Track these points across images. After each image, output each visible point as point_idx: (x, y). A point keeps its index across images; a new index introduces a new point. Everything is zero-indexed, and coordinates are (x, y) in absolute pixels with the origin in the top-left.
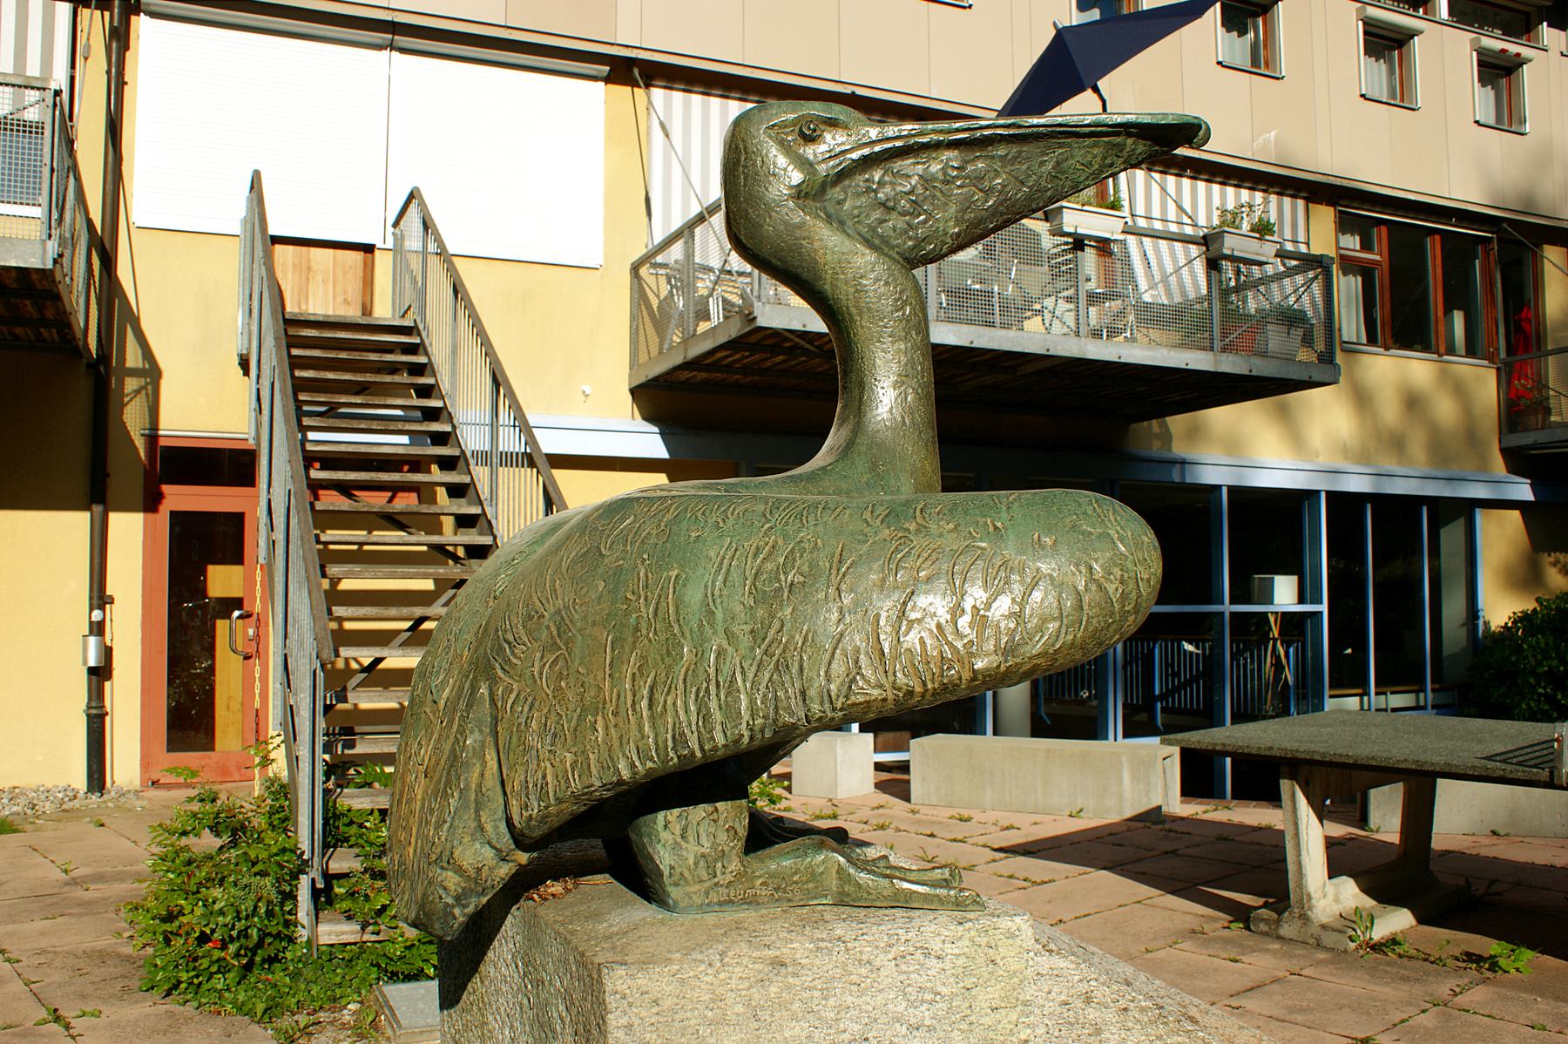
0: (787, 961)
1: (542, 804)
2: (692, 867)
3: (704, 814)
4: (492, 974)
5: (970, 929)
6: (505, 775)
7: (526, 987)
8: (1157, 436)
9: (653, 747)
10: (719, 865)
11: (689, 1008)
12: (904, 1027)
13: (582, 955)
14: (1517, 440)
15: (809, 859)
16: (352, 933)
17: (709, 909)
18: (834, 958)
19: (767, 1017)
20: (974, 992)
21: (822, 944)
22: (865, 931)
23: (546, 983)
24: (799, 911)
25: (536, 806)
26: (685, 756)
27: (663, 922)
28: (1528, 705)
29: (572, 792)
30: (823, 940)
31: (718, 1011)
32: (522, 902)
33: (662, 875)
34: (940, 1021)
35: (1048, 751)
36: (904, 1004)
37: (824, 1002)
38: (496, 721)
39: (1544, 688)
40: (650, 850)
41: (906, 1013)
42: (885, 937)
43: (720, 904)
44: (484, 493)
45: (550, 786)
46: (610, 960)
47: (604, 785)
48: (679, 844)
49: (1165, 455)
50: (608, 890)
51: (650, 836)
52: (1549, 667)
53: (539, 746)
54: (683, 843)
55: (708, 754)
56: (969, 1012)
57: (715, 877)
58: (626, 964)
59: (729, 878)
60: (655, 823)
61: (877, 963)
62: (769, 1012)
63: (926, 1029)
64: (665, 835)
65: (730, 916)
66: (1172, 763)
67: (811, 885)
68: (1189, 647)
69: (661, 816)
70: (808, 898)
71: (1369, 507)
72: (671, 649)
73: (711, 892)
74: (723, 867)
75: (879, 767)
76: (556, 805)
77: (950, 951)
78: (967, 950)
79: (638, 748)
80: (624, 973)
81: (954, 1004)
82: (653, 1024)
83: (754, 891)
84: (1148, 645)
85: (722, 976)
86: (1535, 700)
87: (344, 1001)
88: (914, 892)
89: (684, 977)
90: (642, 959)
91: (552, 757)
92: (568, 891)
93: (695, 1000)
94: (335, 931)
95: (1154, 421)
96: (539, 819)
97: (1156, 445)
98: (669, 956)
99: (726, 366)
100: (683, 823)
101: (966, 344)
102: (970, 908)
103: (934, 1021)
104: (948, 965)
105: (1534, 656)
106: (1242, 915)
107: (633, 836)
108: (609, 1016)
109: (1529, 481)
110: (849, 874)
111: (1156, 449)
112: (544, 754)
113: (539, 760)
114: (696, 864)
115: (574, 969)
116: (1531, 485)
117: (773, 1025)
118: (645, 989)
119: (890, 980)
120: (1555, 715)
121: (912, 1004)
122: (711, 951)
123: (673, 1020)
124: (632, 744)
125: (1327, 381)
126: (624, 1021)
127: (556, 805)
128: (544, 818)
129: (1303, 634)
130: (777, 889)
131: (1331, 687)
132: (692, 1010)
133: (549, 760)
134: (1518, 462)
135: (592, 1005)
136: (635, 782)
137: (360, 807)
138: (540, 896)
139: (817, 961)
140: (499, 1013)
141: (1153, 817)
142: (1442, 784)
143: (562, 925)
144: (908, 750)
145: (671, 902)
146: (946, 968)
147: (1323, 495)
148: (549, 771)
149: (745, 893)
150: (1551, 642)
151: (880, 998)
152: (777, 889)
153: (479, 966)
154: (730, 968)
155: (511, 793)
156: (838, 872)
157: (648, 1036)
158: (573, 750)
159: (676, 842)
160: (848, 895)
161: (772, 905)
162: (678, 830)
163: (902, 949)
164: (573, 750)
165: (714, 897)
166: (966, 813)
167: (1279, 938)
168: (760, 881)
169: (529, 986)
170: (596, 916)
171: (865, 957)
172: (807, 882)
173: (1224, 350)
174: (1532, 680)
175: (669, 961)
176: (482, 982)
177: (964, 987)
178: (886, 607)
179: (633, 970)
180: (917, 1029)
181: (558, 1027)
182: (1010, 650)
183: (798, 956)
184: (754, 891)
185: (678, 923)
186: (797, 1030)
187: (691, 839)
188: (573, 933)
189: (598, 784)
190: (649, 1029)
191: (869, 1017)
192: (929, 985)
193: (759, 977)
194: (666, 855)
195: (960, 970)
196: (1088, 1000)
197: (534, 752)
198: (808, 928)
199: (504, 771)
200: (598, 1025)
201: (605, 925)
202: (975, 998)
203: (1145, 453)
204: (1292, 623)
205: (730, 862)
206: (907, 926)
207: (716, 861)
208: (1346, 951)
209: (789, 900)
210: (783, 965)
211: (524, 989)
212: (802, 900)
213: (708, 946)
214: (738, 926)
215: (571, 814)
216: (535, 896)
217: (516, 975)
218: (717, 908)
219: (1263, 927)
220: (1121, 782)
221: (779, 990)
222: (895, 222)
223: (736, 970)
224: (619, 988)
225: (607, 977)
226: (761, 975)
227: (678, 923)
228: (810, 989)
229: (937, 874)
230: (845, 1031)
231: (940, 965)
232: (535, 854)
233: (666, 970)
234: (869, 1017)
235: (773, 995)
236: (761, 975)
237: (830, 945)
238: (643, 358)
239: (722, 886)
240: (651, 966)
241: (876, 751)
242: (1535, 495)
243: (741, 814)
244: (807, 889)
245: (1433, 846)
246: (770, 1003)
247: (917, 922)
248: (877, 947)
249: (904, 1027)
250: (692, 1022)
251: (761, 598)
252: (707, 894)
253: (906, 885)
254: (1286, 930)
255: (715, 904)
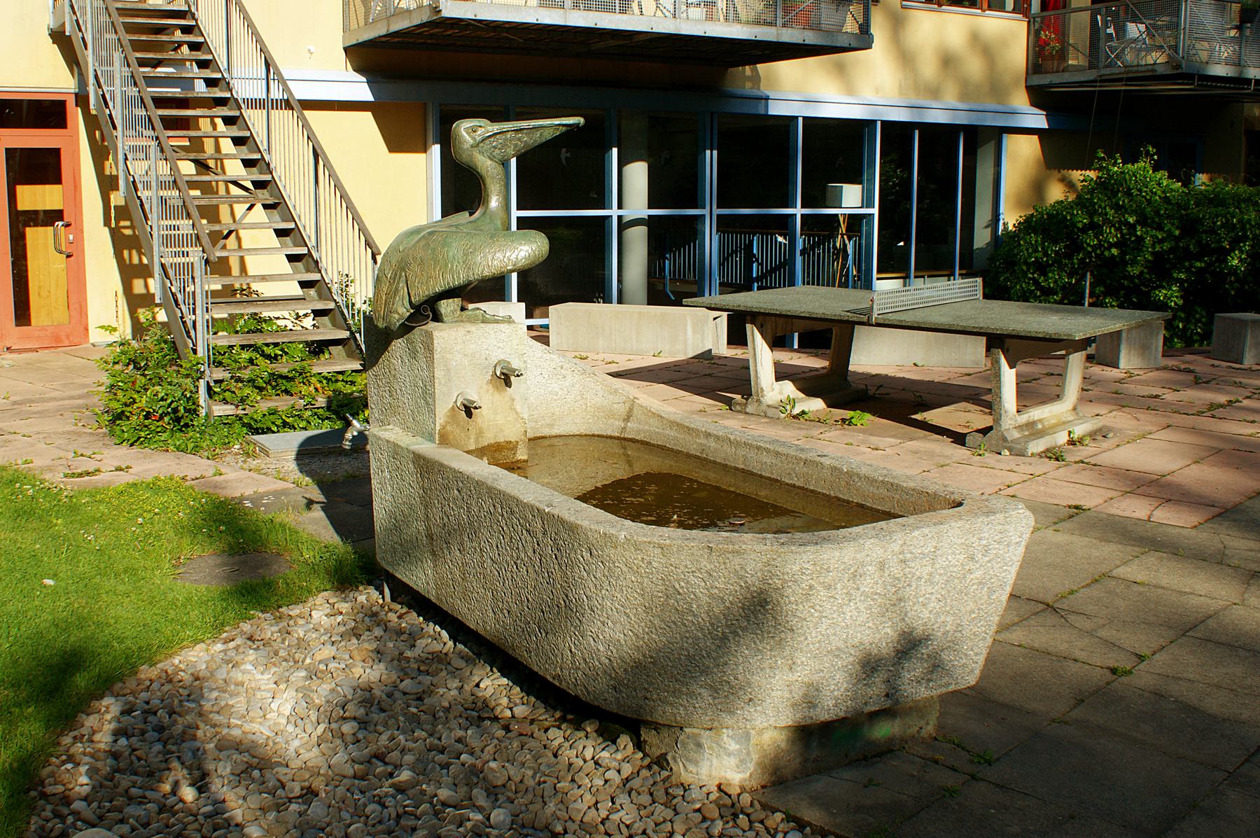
8: (749, 79)
14: (1039, 80)
16: (231, 409)
28: (1021, 286)
35: (640, 313)
38: (407, 281)
39: (1033, 274)
44: (262, 145)
49: (755, 93)
52: (1036, 258)
66: (721, 321)
68: (780, 239)
71: (917, 132)
72: (446, 266)
84: (749, 237)
86: (1026, 283)
87: (231, 444)
94: (220, 410)
95: (747, 67)
97: (748, 85)
99: (418, 34)
101: (593, 26)
105: (1027, 250)
106: (729, 402)
109: (1044, 113)
111: (748, 89)
116: (1046, 115)
120: (1038, 294)
125: (861, 47)
129: (860, 231)
131: (878, 272)
134: (1039, 97)
137: (222, 344)
141: (706, 356)
142: (21, 207)
144: (519, 301)
147: (879, 124)
150: (1039, 239)
166: (584, 355)
167: (746, 413)
173: (784, 25)
174: (1024, 268)
178: (490, 257)
182: (514, 265)
196: (562, 368)
203: (739, 91)
204: (855, 222)
208: (778, 419)
219: (738, 408)
220: (686, 333)
222: (497, 151)
238: (354, 26)
242: (1049, 125)
245: (851, 368)
251: (465, 255)
254: (749, 409)
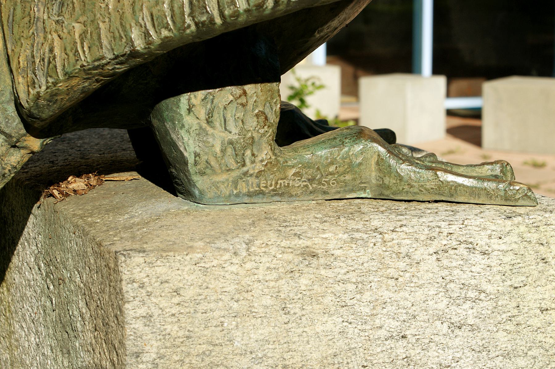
0: (319, 252)
1: (51, 80)
2: (219, 154)
3: (231, 98)
4: (17, 281)
5: (519, 224)
6: (10, 51)
7: (48, 288)
9: (168, 13)
10: (248, 153)
11: (213, 298)
12: (446, 325)
13: (100, 245)
15: (346, 149)
17: (238, 200)
18: (370, 250)
19: (297, 310)
20: (522, 291)
21: (357, 235)
22: (404, 223)
23: (67, 281)
24: (335, 204)
25: (44, 82)
26: (203, 23)
27: (187, 213)
29: (83, 66)
30: (358, 231)
31: (243, 302)
32: (42, 199)
33: (186, 163)
34: (484, 320)
36: (446, 301)
37: (358, 296)
40: (174, 136)
41: (447, 310)
42: (426, 230)
43: (250, 195)
45: (58, 59)
46: (127, 248)
47: (116, 57)
48: (204, 130)
50: (134, 185)
51: (173, 121)
53: (46, 17)
54: (208, 128)
55: (228, 20)
56: (515, 312)
57: (244, 165)
58: (144, 252)
59: (259, 167)
60: (178, 107)
61: (417, 256)
62: (300, 306)
63: (469, 328)
64: (188, 120)
65: (258, 208)
67: (348, 177)
69: (184, 99)
70: (345, 191)
73: (240, 182)
74: (253, 155)
75: (450, 113)
76: (65, 81)
77: (496, 247)
78: (514, 246)
79: (152, 15)
80: (141, 260)
81: (500, 303)
82: (173, 315)
83: (287, 182)
85: (248, 266)
88: (460, 185)
89: (207, 266)
90: (162, 246)
91: (59, 28)
92: (90, 187)
93: (219, 291)
96: (48, 97)
98: (191, 244)
100: (209, 106)
102: (520, 203)
103: (477, 320)
104: (494, 262)
107: (155, 122)
108: (127, 306)
110: (389, 166)
112: (51, 25)
113: (45, 32)
114: (223, 151)
115: (92, 261)
117: (304, 318)
118: (164, 278)
119: (431, 275)
121: (453, 301)
122: (237, 240)
123: (196, 311)
124: (145, 11)
126: (142, 311)
127: (65, 81)
128: (53, 96)
130: (311, 180)
132: (217, 301)
133: (56, 31)
135: (110, 296)
136: (150, 53)
138: (61, 193)
139: (352, 253)
140: (25, 320)
143: (81, 218)
145: (197, 192)
146: (492, 264)
148: (57, 43)
149: (277, 183)
151: (419, 295)
152: (311, 180)
153: (4, 274)
154: (257, 258)
155: (17, 70)
156: (378, 163)
157: (169, 327)
158: (82, 19)
159: (201, 128)
160: (388, 188)
161: (306, 198)
162: (202, 114)
163: (444, 242)
164: (82, 19)
165: (243, 188)
166: (540, 159)
168: (293, 171)
169: (51, 287)
170: (117, 209)
171: (403, 250)
172: (344, 173)
175: (190, 249)
176: (8, 290)
177: (511, 286)
179: (151, 258)
180: (460, 328)
181: (78, 325)
183: (331, 246)
184: (287, 182)
185: (204, 213)
186: (329, 326)
187: (217, 124)
188: (91, 225)
189: (109, 56)
190: (169, 320)
191: (406, 313)
192: (473, 282)
193: (288, 268)
194: (191, 142)
195: (508, 267)
197: (40, 24)
198: (343, 219)
199: (9, 46)
200: (116, 316)
201: (126, 216)
202: (523, 297)
205: (260, 150)
206: (450, 218)
207: (245, 148)
209: (325, 193)
210: (314, 255)
211: (46, 290)
212: (339, 193)
213: (234, 235)
214: (268, 217)
215: (83, 92)
216: (56, 192)
217: (39, 278)
218: (246, 199)
221: (310, 283)
223: (264, 260)
224: (137, 276)
225: (123, 264)
226: (291, 266)
227: (204, 213)
228: (344, 282)
229: (486, 170)
230: (381, 328)
231: (486, 261)
232: (48, 141)
233: (188, 258)
234: (406, 313)
235: (303, 288)
236: (291, 266)
237: (365, 236)
239: (251, 175)
240: (171, 254)
241: (449, 95)
243: (272, 98)
244: (344, 181)
246: (300, 296)
247: (461, 216)
248: (417, 240)
249: (446, 325)
250: (217, 314)
252: (235, 183)
253: (450, 178)
255: (244, 195)
